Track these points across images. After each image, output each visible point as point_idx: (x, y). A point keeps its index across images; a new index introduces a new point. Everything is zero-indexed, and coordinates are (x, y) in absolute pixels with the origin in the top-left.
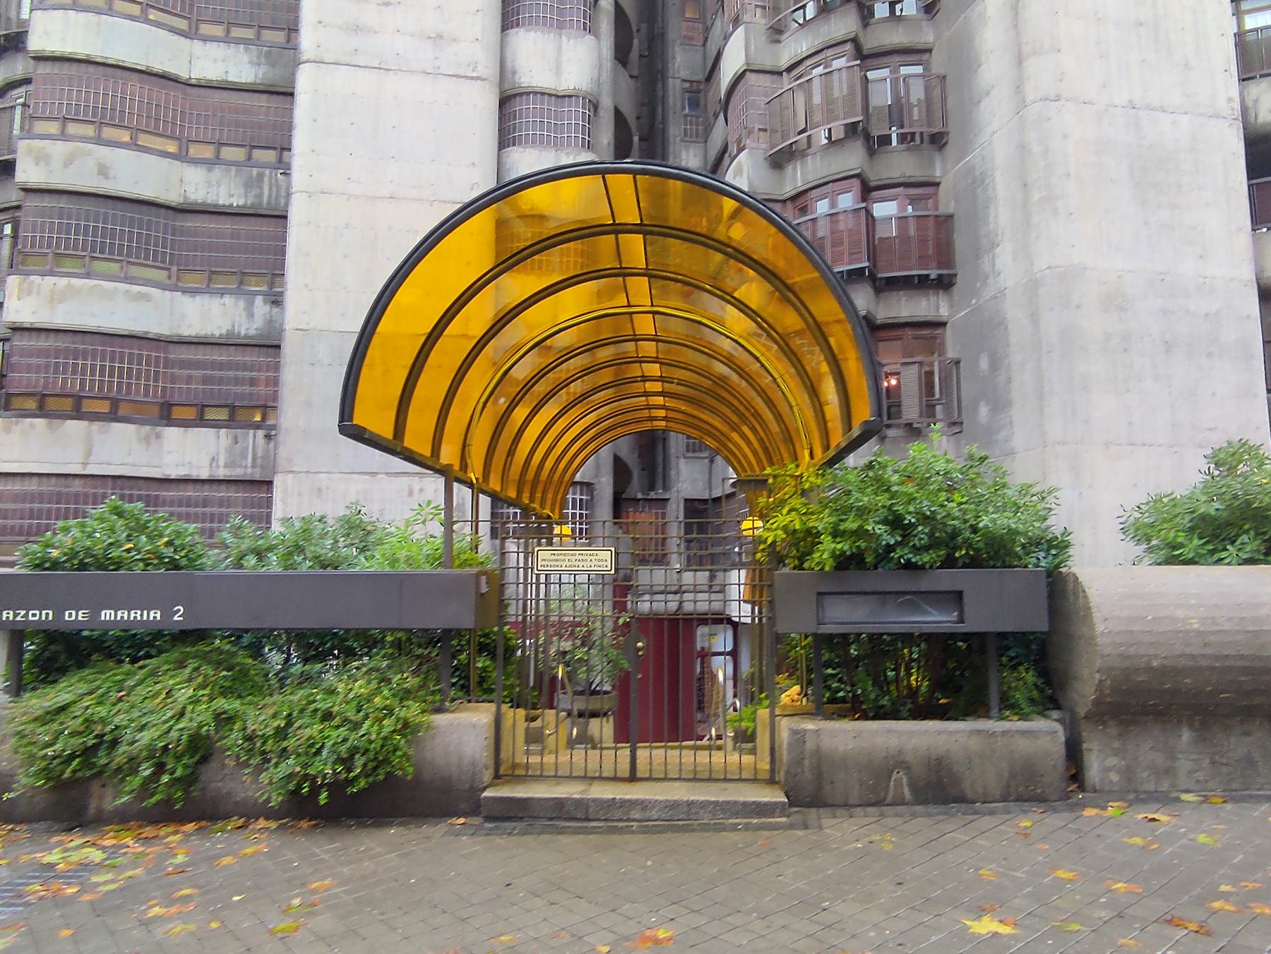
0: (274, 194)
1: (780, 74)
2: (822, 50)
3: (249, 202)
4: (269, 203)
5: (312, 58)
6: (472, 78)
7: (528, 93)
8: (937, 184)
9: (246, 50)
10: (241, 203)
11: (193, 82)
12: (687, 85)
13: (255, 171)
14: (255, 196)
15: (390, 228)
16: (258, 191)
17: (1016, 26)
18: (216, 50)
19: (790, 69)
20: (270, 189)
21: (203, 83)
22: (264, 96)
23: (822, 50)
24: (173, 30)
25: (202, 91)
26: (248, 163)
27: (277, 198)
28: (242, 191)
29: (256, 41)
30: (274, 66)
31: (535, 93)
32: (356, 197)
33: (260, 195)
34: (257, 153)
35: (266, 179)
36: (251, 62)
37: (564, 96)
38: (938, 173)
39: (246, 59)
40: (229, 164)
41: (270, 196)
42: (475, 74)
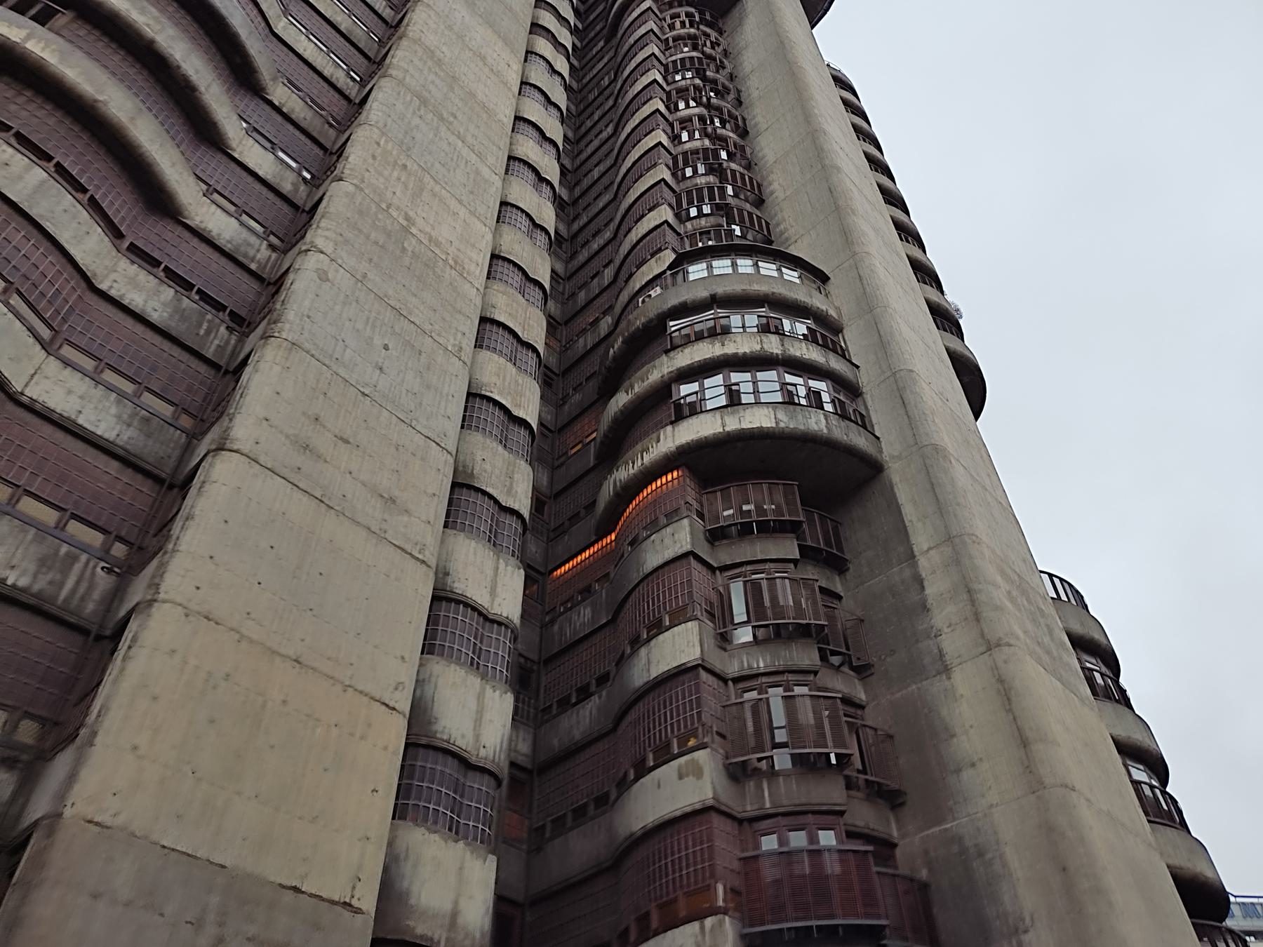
0: (82, 590)
1: (725, 681)
2: (782, 672)
3: (36, 588)
4: (66, 600)
5: (245, 451)
6: (417, 559)
7: (458, 602)
8: (894, 846)
9: (118, 402)
10: (22, 582)
11: (24, 399)
12: (522, 660)
13: (64, 549)
14: (50, 583)
15: (284, 702)
16: (58, 577)
17: (1010, 711)
18: (80, 384)
19: (736, 680)
20: (78, 583)
21: (38, 407)
22: (115, 464)
23: (782, 672)
24: (31, 330)
25: (28, 417)
26: (57, 532)
27: (83, 599)
28: (32, 567)
29: (134, 399)
30: (149, 436)
31: (466, 605)
32: (251, 641)
33: (61, 585)
34: (74, 527)
35: (77, 567)
36: (119, 417)
37: (493, 621)
38: (895, 833)
39: (113, 410)
40: (27, 521)
41: (74, 591)
42: (420, 557)
